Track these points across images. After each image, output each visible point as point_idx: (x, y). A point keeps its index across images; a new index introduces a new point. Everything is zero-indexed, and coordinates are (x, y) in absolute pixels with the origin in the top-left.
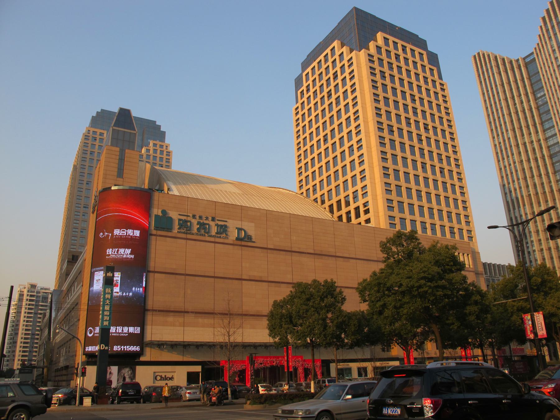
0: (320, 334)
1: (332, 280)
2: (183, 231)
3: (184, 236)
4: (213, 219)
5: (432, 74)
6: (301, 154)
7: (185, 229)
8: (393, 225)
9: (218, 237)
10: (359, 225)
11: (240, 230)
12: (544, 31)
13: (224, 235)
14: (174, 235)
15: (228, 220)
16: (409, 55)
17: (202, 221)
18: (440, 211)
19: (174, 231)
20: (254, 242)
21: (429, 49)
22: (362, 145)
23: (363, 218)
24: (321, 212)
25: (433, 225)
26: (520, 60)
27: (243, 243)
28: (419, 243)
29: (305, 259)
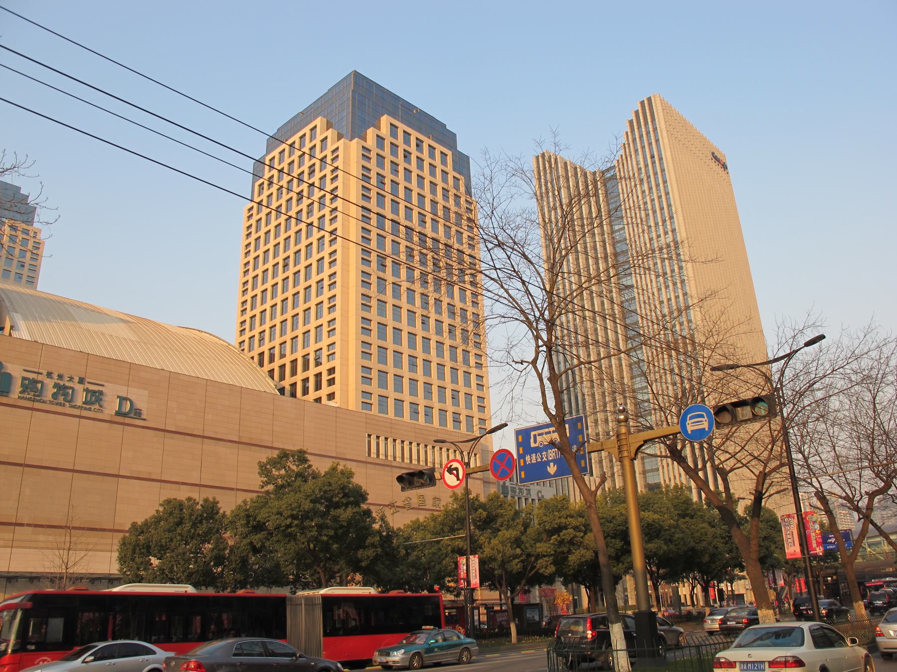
0: (265, 561)
1: (214, 498)
2: (28, 396)
3: (29, 404)
4: (81, 381)
5: (457, 187)
6: (247, 281)
7: (32, 393)
8: (367, 405)
9: (86, 409)
10: (318, 404)
11: (123, 399)
12: (630, 140)
13: (97, 406)
14: (11, 402)
15: (105, 384)
16: (425, 155)
17: (62, 383)
18: (442, 388)
19: (13, 396)
20: (145, 420)
21: (460, 148)
22: (335, 282)
23: (325, 390)
24: (259, 377)
25: (429, 408)
26: (598, 173)
27: (127, 420)
28: (310, 466)
29: (222, 449)
